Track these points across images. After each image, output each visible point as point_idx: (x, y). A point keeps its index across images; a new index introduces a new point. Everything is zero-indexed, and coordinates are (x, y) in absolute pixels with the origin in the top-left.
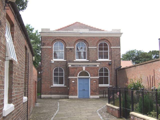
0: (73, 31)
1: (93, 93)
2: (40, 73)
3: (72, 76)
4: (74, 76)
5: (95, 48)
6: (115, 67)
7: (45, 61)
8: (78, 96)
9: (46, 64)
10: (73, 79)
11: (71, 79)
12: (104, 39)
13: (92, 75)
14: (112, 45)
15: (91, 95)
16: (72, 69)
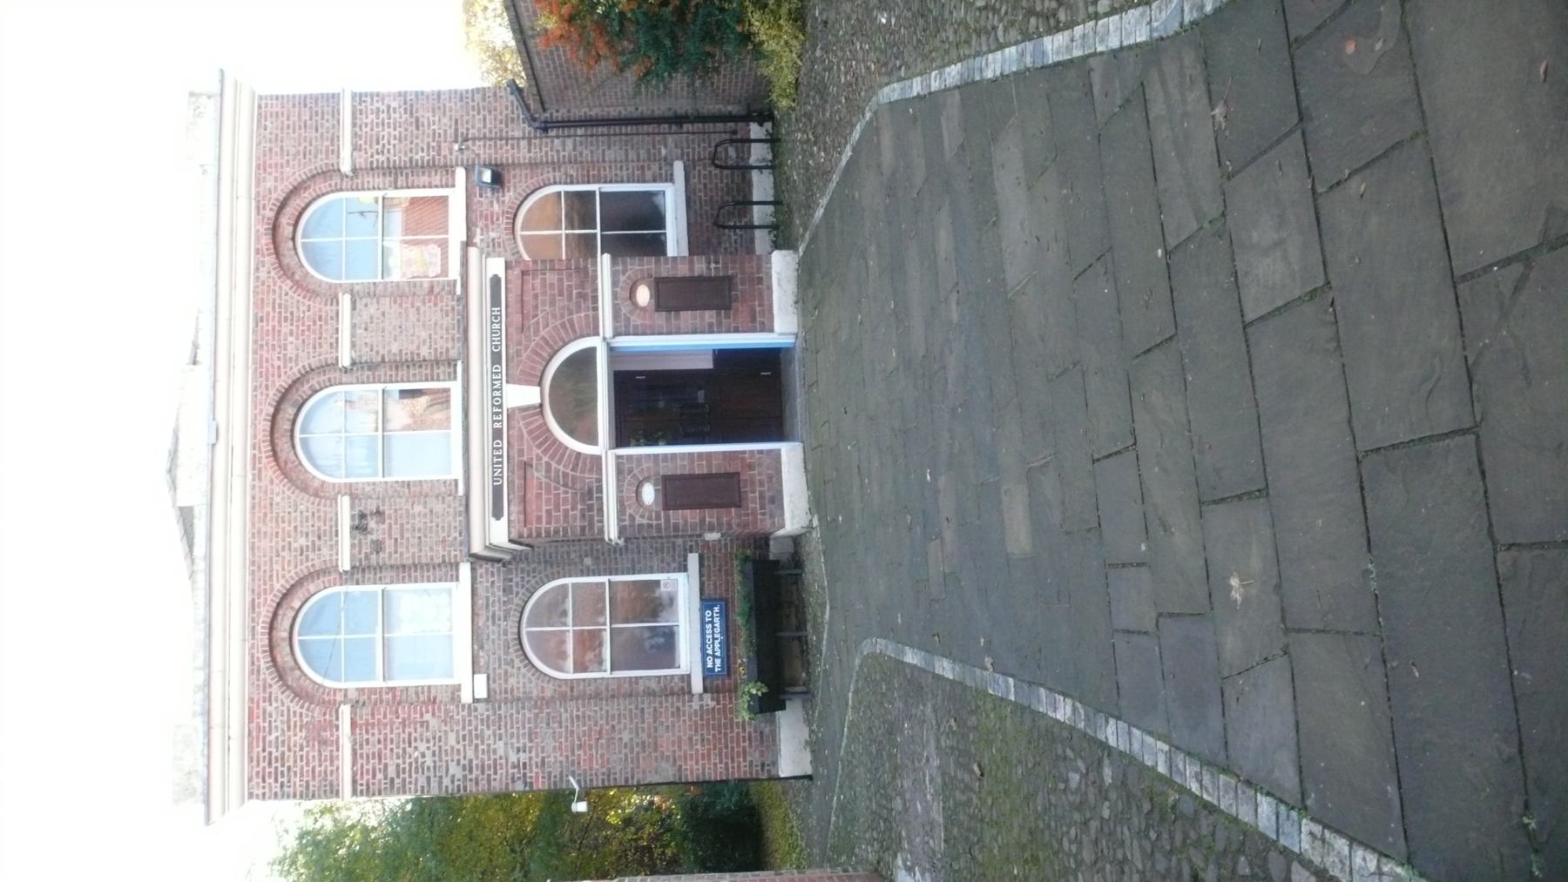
0: (196, 512)
2: (579, 799)
3: (600, 510)
4: (600, 490)
5: (354, 308)
6: (517, 134)
7: (470, 754)
10: (621, 503)
12: (275, 229)
14: (320, 163)
15: (771, 330)
16: (532, 507)
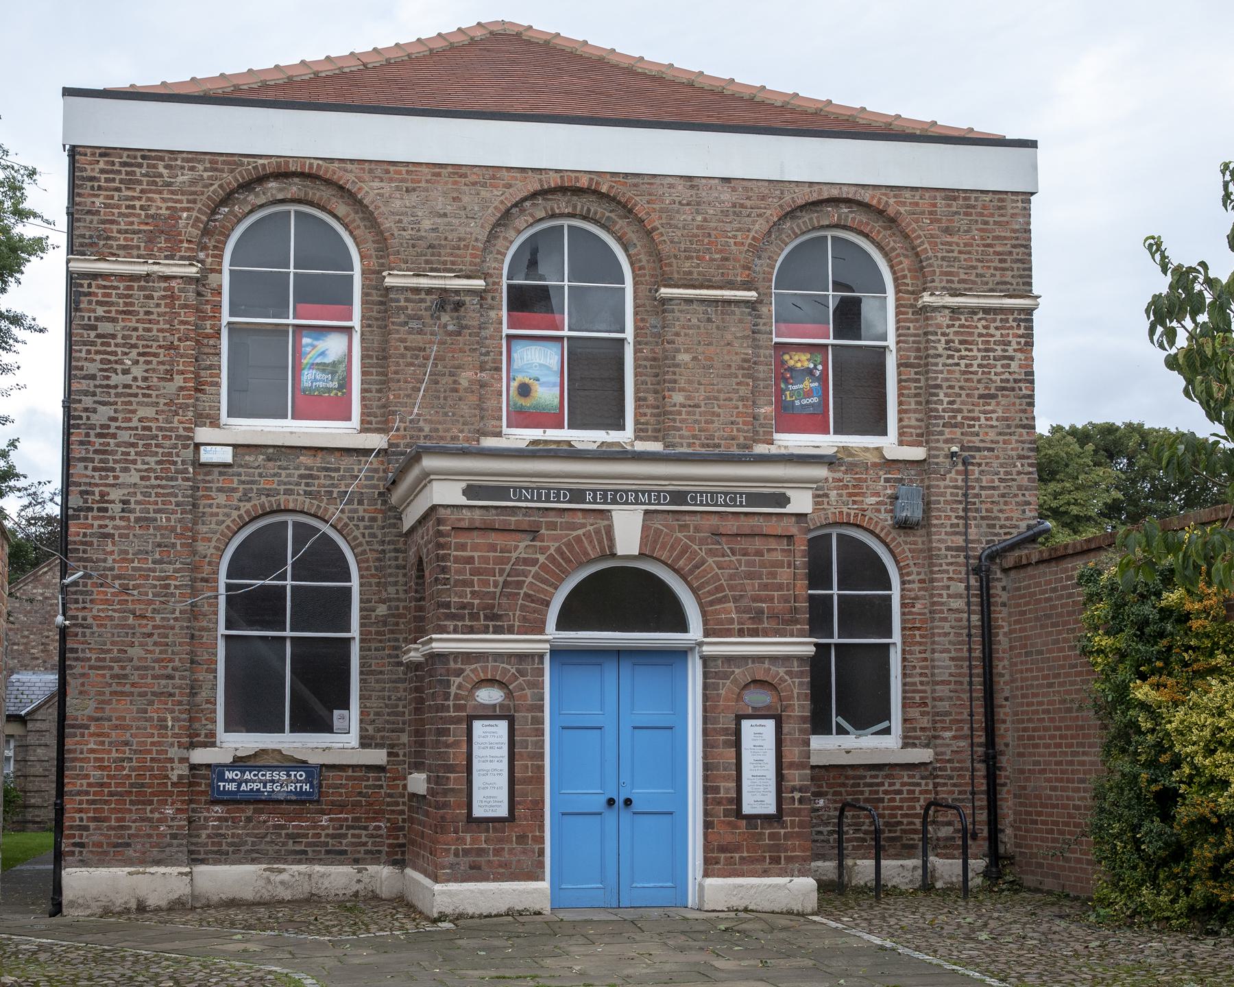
1: (737, 848)
3: (471, 630)
4: (498, 630)
7: (124, 436)
8: (545, 885)
9: (134, 478)
11: (468, 657)
13: (730, 611)
14: (936, 266)
15: (706, 874)
16: (477, 538)
